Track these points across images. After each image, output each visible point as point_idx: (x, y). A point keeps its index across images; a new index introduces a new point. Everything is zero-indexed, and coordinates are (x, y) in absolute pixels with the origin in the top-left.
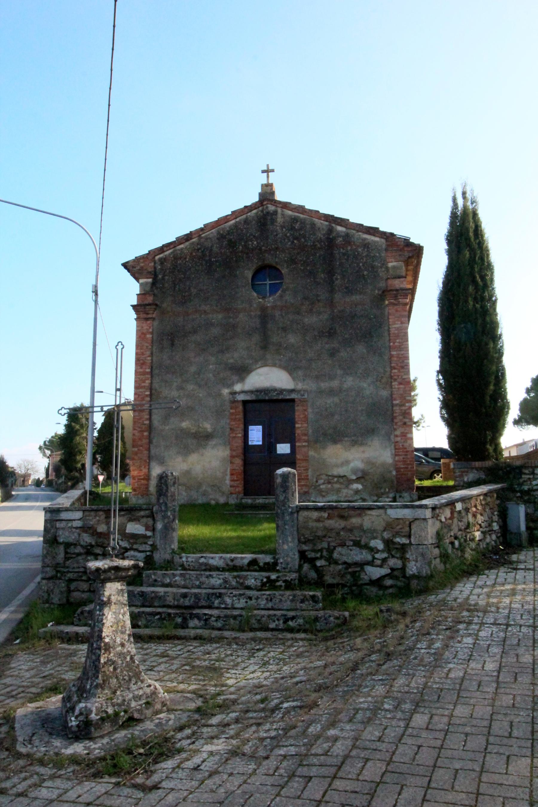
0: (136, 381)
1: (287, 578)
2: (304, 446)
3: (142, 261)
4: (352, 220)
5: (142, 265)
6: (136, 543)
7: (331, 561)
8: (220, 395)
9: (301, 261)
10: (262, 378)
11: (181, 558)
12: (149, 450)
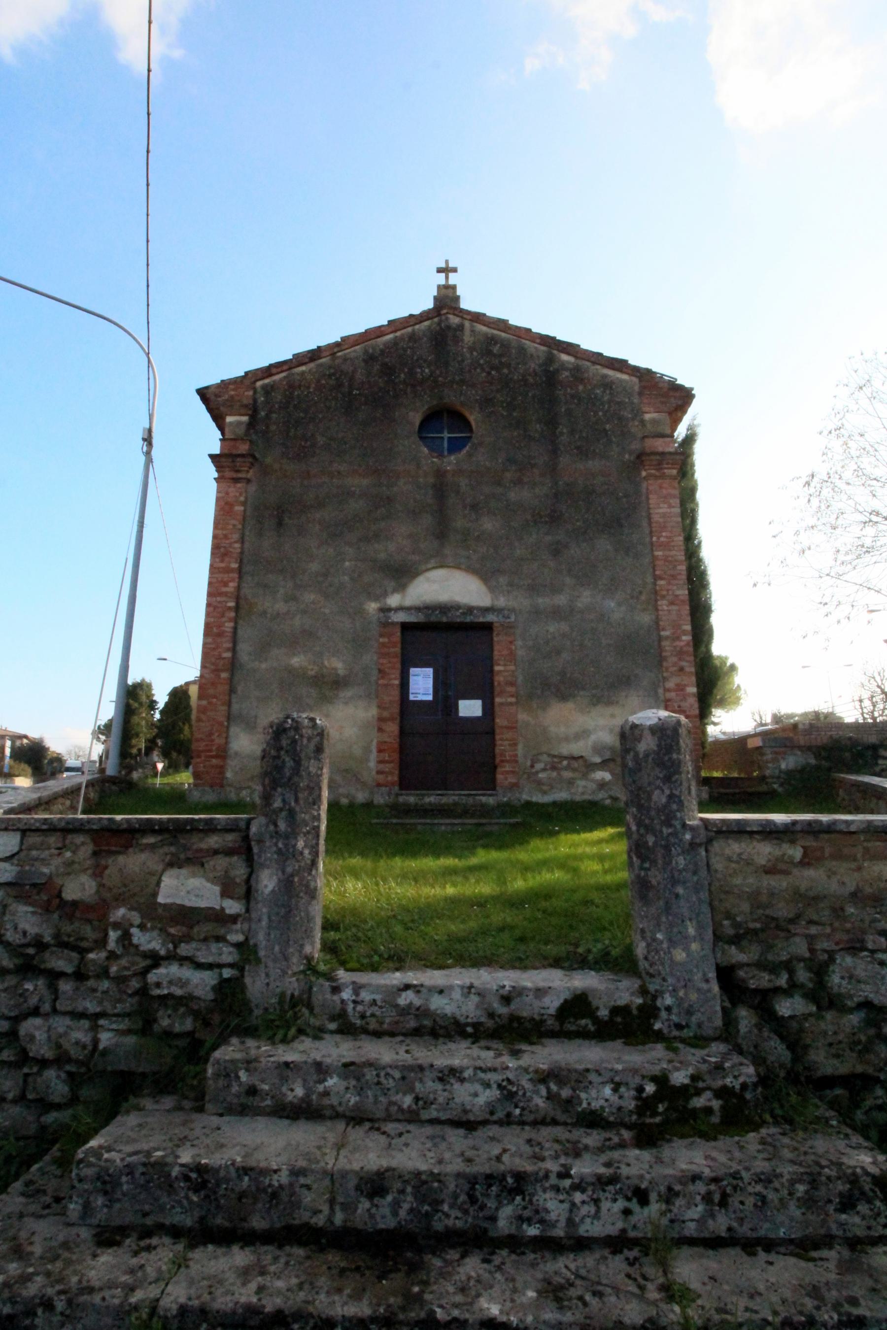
0: (210, 584)
1: (728, 1081)
2: (511, 704)
3: (231, 387)
4: (584, 346)
5: (232, 393)
6: (187, 938)
7: (824, 999)
8: (360, 612)
9: (502, 402)
10: (435, 587)
11: (336, 990)
12: (229, 704)
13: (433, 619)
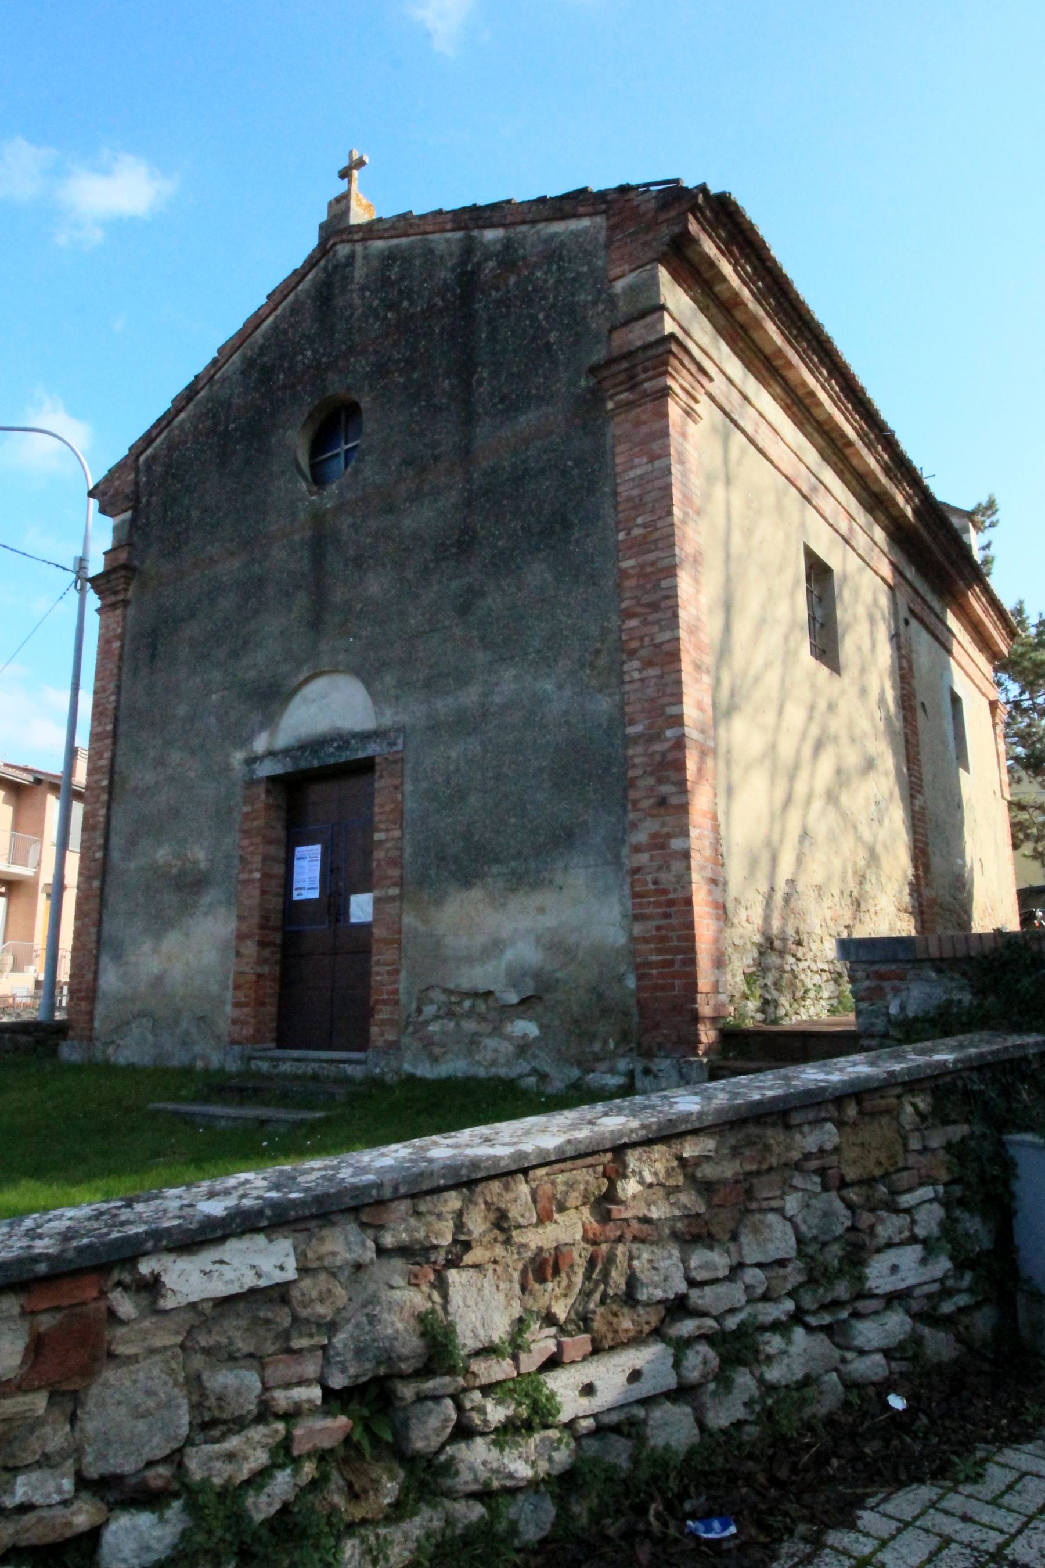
10: (313, 709)
13: (303, 764)
